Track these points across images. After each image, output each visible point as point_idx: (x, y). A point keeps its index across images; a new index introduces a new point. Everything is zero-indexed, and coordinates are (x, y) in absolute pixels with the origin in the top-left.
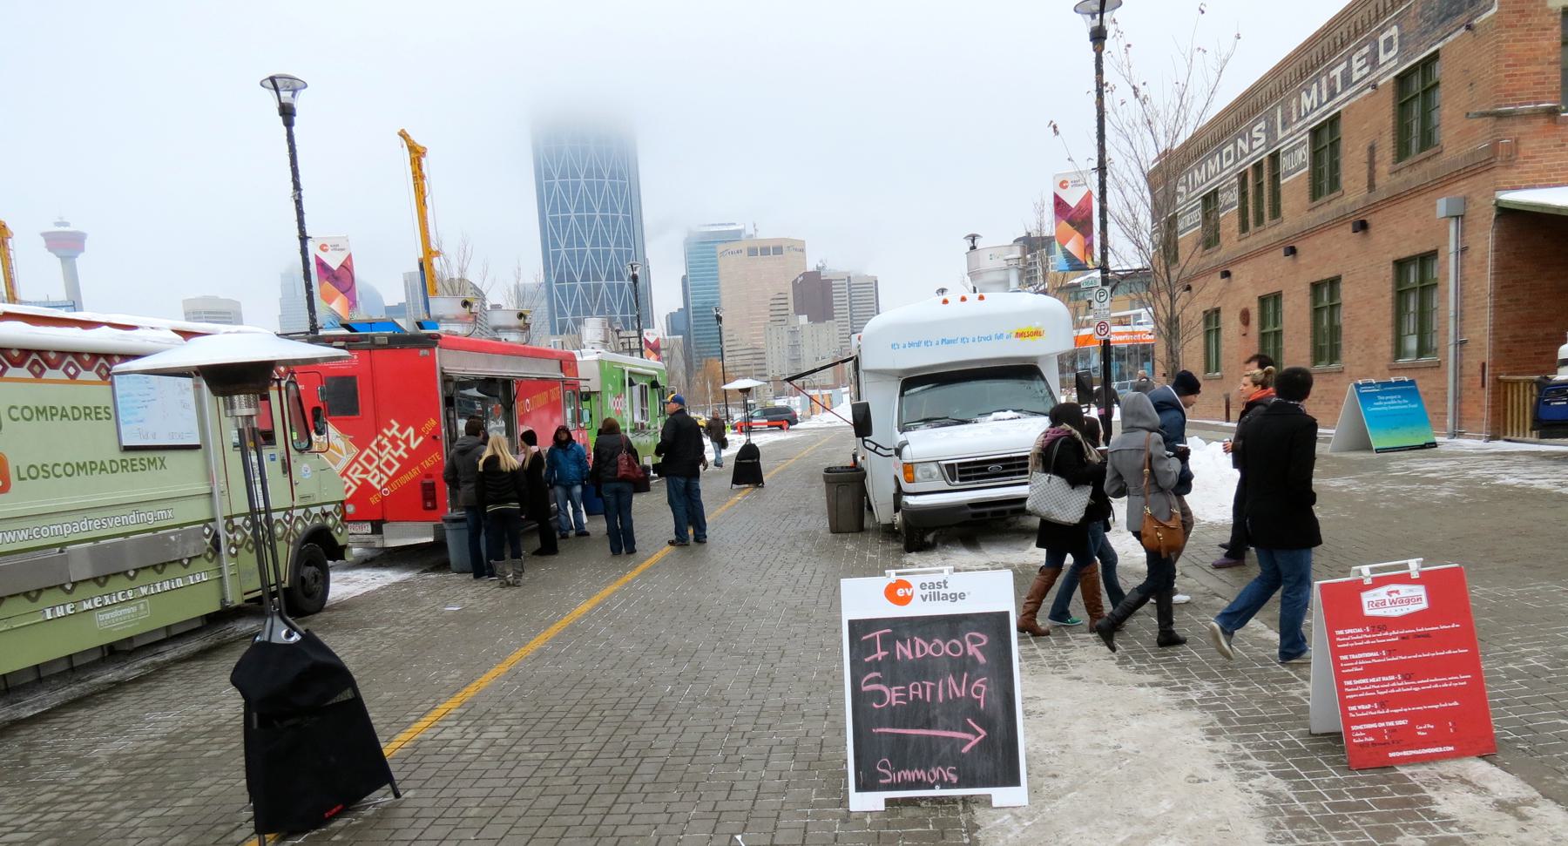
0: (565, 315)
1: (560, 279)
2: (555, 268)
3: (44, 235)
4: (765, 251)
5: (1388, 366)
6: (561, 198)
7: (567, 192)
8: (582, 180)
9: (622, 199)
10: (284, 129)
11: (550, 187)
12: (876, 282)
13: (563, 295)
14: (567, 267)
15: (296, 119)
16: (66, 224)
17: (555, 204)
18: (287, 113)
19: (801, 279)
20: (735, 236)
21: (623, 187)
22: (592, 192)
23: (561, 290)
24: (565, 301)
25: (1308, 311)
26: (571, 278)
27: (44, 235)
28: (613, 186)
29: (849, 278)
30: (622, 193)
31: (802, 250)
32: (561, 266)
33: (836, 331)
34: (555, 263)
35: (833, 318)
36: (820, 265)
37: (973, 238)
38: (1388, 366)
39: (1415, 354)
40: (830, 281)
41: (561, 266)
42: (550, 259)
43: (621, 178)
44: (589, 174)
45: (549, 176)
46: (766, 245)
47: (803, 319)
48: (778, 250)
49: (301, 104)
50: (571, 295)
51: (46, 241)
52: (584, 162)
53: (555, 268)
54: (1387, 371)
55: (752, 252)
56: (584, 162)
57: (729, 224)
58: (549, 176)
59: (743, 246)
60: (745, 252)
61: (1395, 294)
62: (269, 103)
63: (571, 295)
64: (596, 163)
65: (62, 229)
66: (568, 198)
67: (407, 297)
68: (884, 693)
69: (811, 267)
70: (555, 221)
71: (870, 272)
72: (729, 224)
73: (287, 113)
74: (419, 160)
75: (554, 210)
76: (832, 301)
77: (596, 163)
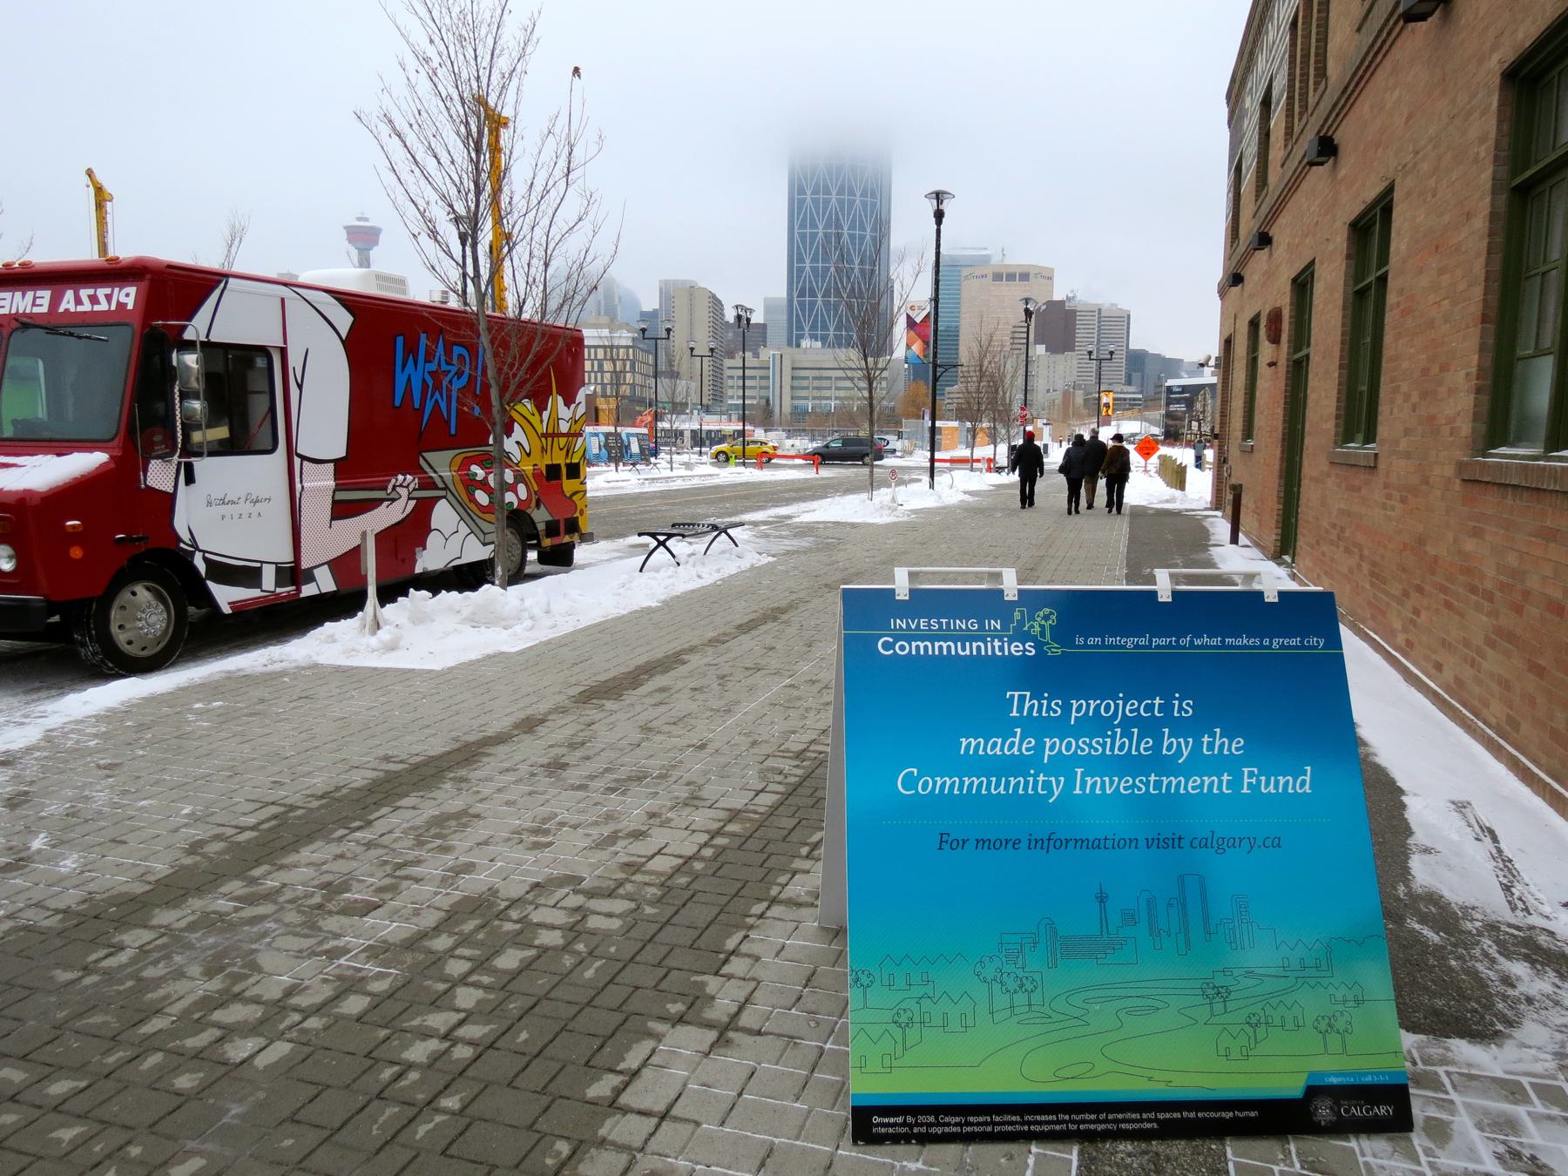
0: (803, 329)
1: (802, 294)
2: (798, 283)
3: (345, 228)
4: (1011, 277)
5: (1461, 467)
6: (811, 213)
7: (817, 208)
8: (834, 197)
9: (871, 217)
10: (935, 227)
11: (801, 202)
12: (1129, 316)
13: (803, 310)
14: (810, 282)
15: (944, 220)
16: (366, 220)
17: (804, 220)
18: (939, 215)
19: (1044, 307)
20: (985, 260)
21: (873, 205)
22: (817, 208)
23: (802, 304)
24: (804, 316)
25: (1340, 302)
26: (813, 294)
27: (345, 228)
28: (864, 204)
29: (1100, 310)
30: (872, 212)
31: (1050, 278)
32: (804, 282)
33: (1075, 362)
34: (799, 277)
35: (1074, 351)
36: (1071, 295)
37: (939, 196)
38: (1461, 467)
39: (1542, 432)
40: (1074, 312)
41: (804, 282)
42: (794, 274)
43: (873, 196)
44: (841, 191)
45: (802, 191)
46: (1010, 270)
47: (1040, 349)
48: (1025, 277)
49: (947, 206)
50: (811, 310)
51: (348, 234)
52: (837, 180)
53: (798, 283)
54: (1457, 485)
55: (998, 277)
56: (837, 180)
57: (981, 249)
58: (802, 191)
59: (989, 272)
60: (990, 277)
61: (1503, 199)
62: (930, 207)
63: (811, 310)
64: (824, 179)
65: (362, 223)
66: (818, 214)
67: (660, 304)
68: (904, 789)
69: (1058, 296)
70: (803, 236)
71: (1123, 305)
72: (981, 249)
73: (939, 215)
74: (497, 130)
75: (802, 226)
76: (1075, 333)
77: (824, 179)
